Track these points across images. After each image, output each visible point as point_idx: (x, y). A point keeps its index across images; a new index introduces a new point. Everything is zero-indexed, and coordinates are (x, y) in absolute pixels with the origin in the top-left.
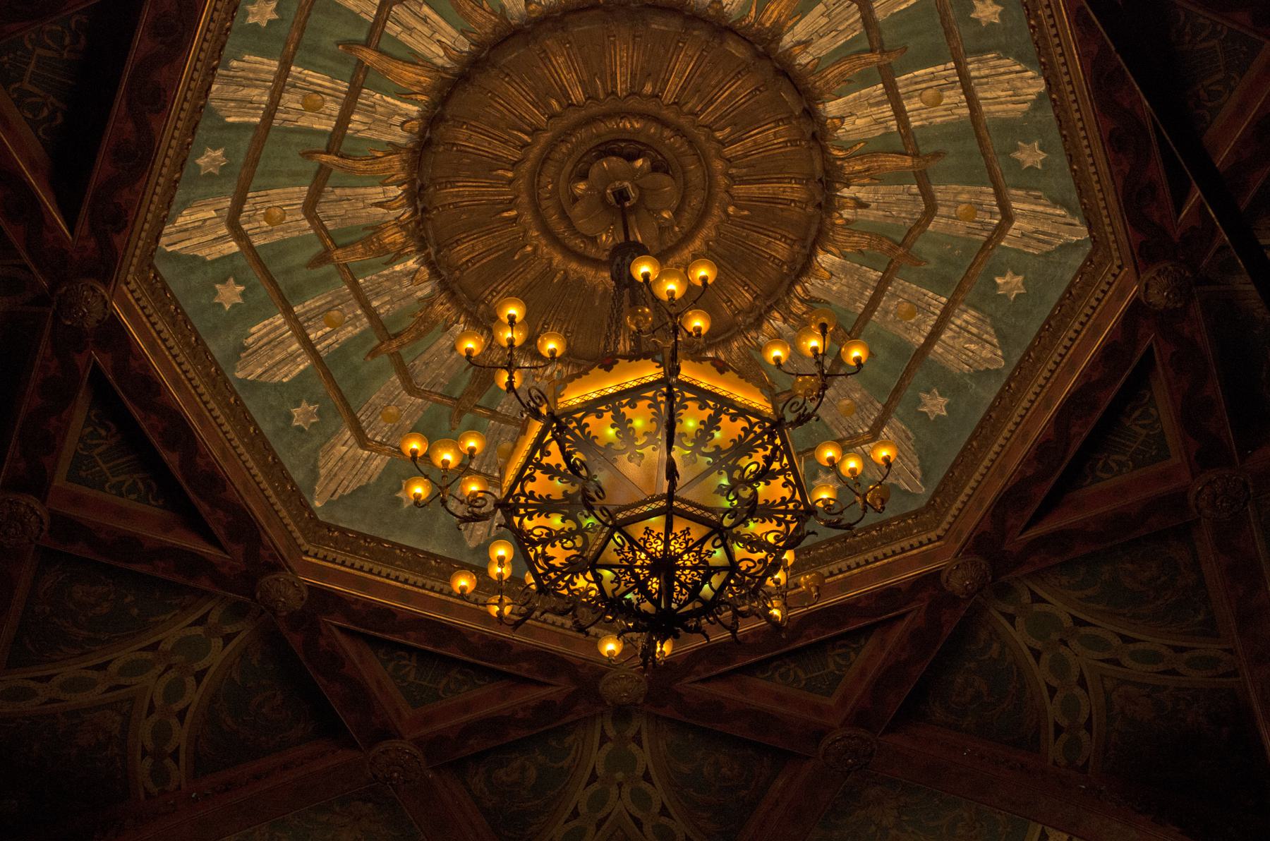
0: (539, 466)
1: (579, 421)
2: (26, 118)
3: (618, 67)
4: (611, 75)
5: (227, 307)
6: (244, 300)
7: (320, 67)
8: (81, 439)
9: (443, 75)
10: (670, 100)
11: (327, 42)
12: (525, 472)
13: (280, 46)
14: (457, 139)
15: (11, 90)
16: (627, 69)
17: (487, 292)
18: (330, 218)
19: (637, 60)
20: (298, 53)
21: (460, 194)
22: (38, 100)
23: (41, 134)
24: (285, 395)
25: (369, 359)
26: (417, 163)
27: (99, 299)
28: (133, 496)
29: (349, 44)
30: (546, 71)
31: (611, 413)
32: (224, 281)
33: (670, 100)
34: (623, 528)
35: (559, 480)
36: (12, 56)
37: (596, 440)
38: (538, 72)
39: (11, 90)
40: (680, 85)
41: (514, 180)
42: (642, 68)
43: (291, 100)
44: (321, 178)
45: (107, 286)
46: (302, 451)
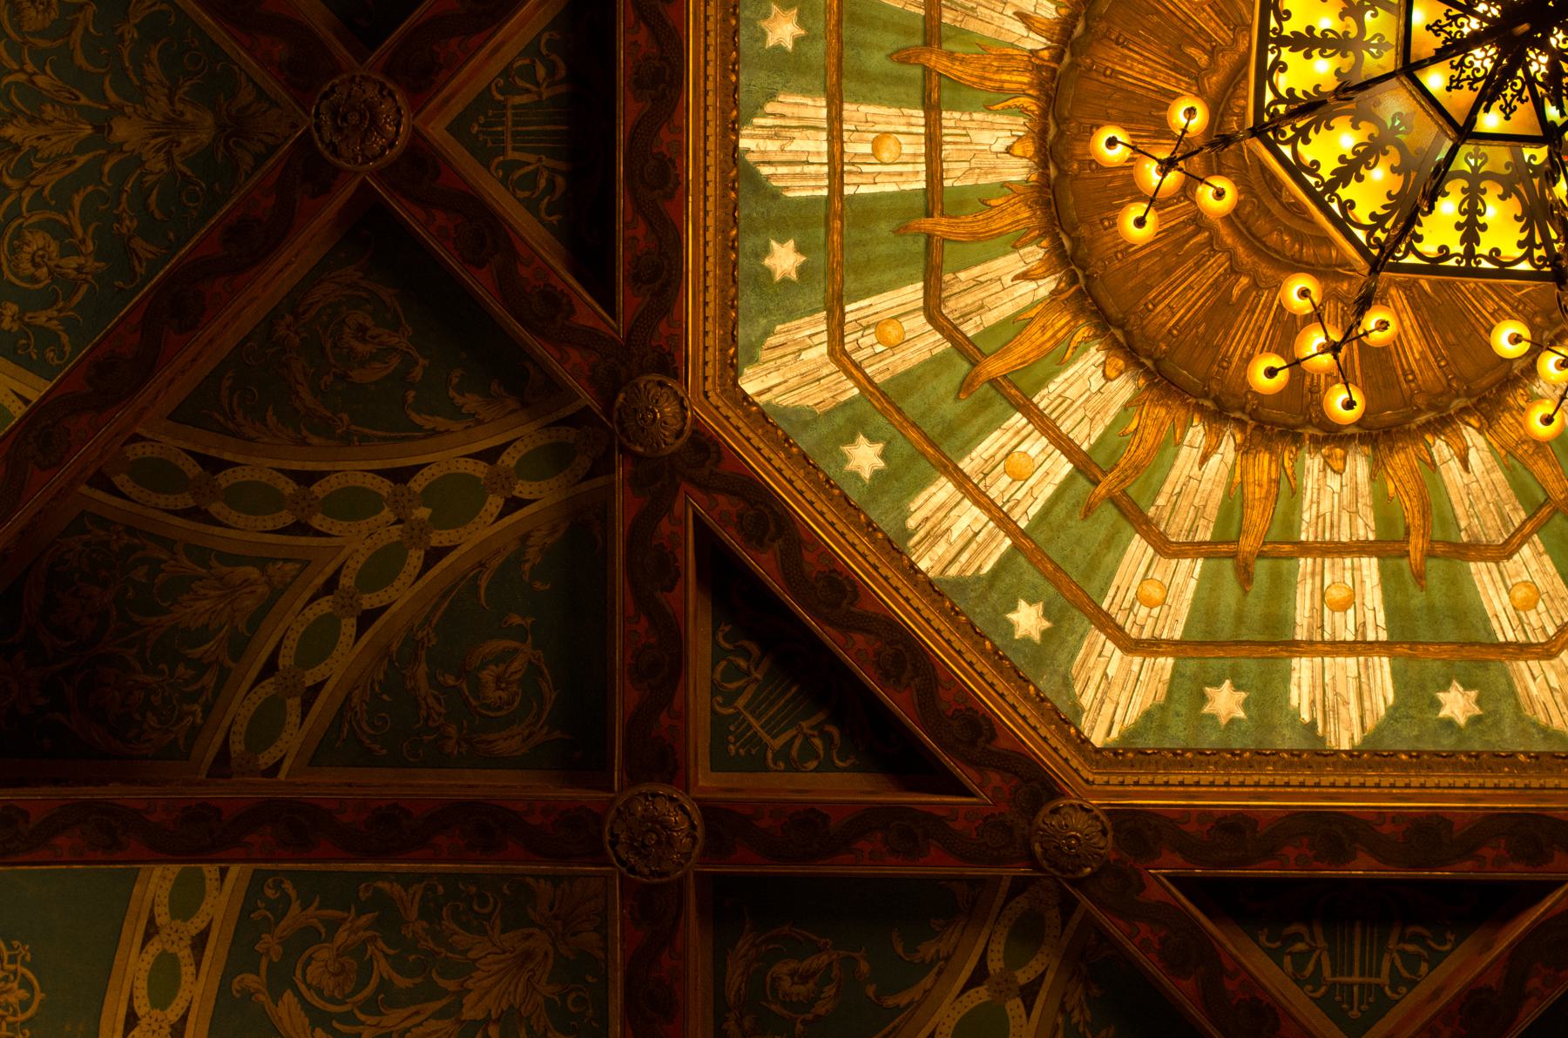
0: (1331, 187)
1: (1528, 256)
2: (815, 770)
3: (1154, 82)
4: (1162, 95)
5: (1241, 714)
6: (885, 461)
7: (978, 434)
8: (1299, 982)
9: (1064, 296)
10: (1228, 35)
11: (950, 409)
12: (1332, 211)
13: (923, 464)
14: (1164, 325)
15: (772, 765)
16: (1160, 71)
17: (1405, 386)
18: (1193, 529)
19: (1154, 54)
20: (945, 448)
21: (1245, 356)
22: (797, 743)
23: (841, 764)
24: (1413, 712)
25: (1424, 583)
26: (1174, 388)
27: (1071, 811)
28: (1424, 967)
29: (966, 386)
30: (1121, 173)
31: (1285, 50)
32: (1203, 699)
33: (1228, 35)
34: (1413, 60)
35: (1368, 168)
36: (731, 738)
37: (1519, 214)
38: (1117, 183)
39: (772, 765)
40: (1213, 14)
41: (1255, 279)
42: (1170, 53)
43: (998, 488)
44: (1136, 517)
45: (1063, 795)
46: (1508, 735)
